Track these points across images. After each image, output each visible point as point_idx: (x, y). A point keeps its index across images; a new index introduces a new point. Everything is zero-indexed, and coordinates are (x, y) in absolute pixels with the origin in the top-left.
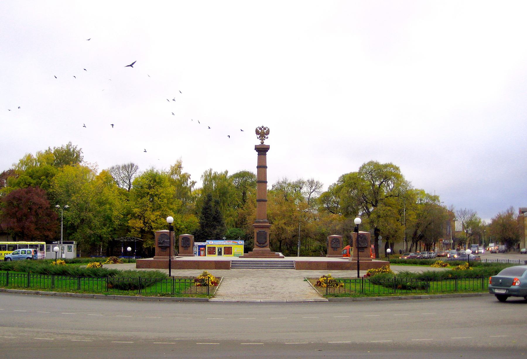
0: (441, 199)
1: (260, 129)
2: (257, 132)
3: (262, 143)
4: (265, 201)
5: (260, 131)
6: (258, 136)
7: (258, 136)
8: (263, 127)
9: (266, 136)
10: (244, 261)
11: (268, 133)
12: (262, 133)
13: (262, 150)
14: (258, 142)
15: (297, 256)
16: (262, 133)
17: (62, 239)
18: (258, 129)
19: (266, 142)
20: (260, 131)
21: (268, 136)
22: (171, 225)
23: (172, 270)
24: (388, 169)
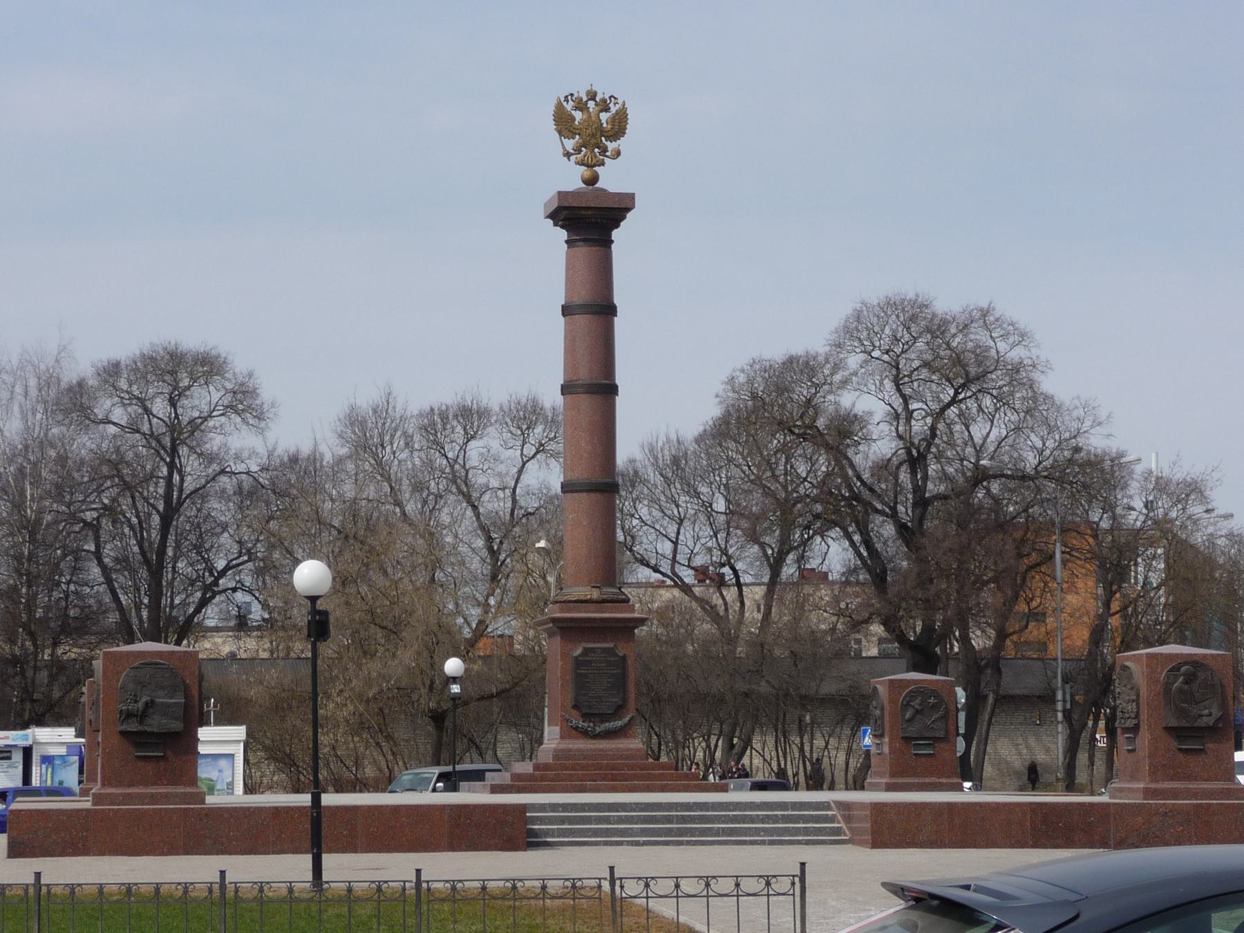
0: (1221, 500)
1: (581, 106)
2: (564, 123)
3: (592, 181)
4: (1232, 516)
5: (578, 115)
6: (570, 144)
7: (570, 144)
8: (592, 96)
9: (611, 146)
10: (554, 807)
11: (619, 127)
12: (593, 128)
13: (590, 221)
14: (571, 178)
15: (822, 789)
16: (593, 128)
17: (836, 825)
18: (569, 106)
19: (613, 178)
20: (578, 115)
21: (622, 143)
22: (320, 605)
23: (326, 858)
24: (979, 335)
